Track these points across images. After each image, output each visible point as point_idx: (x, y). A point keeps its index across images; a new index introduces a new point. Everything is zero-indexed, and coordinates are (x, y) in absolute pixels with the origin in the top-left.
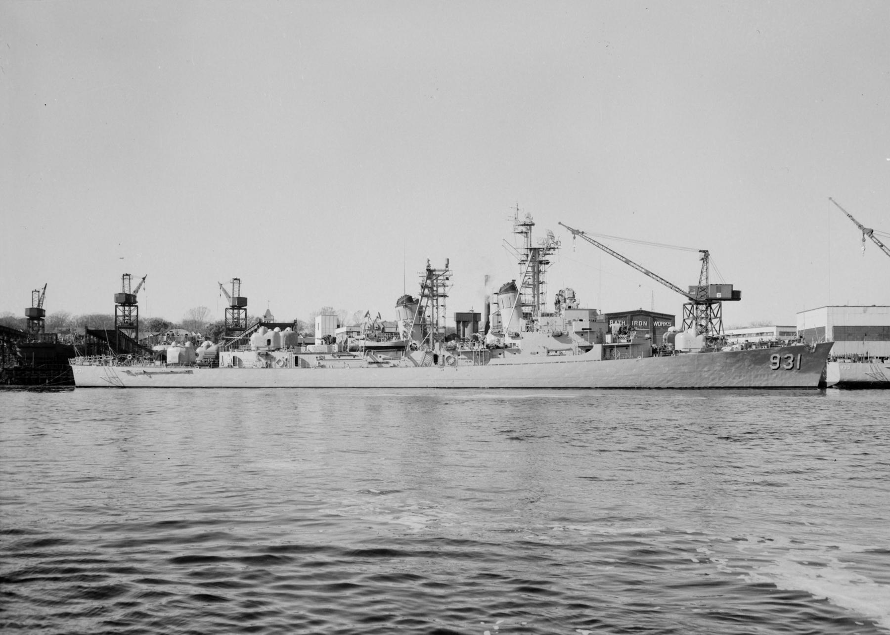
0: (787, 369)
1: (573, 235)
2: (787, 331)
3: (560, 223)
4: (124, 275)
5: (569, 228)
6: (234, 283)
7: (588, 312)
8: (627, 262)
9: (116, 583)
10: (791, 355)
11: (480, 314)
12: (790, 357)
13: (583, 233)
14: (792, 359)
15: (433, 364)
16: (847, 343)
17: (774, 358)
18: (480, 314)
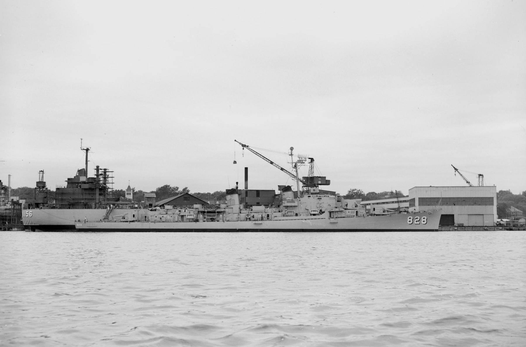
0: (424, 224)
1: (243, 147)
2: (37, 211)
3: (235, 141)
4: (40, 171)
5: (240, 143)
6: (40, 173)
7: (256, 191)
8: (272, 163)
9: (413, 298)
10: (419, 217)
11: (493, 198)
12: (418, 218)
13: (248, 146)
14: (412, 219)
15: (330, 222)
16: (467, 207)
17: (424, 218)
18: (493, 198)
